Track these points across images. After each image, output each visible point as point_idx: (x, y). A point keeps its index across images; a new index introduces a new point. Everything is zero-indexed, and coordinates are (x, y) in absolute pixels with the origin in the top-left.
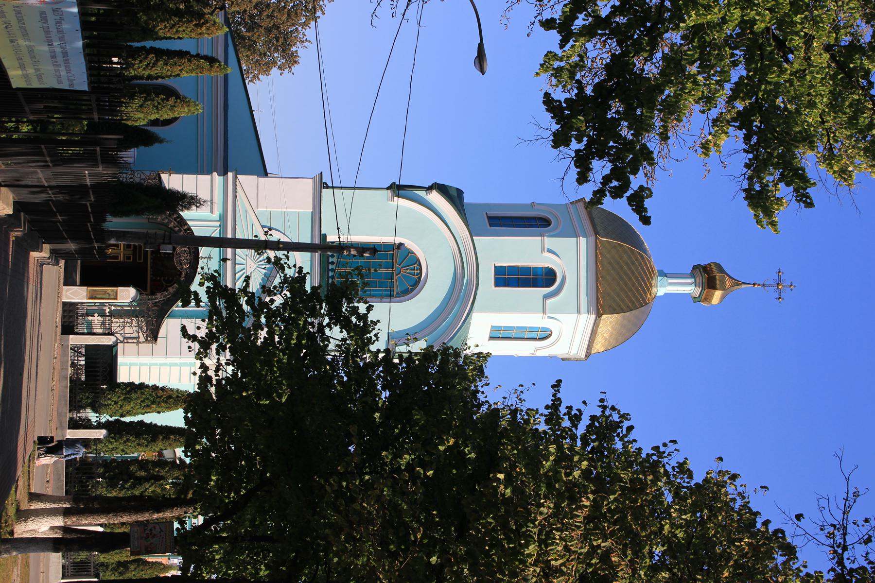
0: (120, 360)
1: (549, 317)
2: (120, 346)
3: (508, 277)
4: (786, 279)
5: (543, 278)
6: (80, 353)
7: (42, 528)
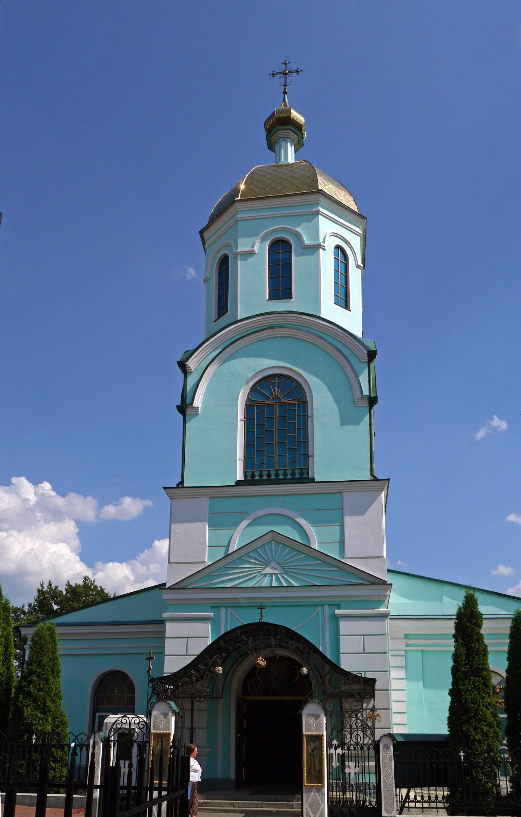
1: (324, 242)
3: (281, 285)
4: (279, 67)
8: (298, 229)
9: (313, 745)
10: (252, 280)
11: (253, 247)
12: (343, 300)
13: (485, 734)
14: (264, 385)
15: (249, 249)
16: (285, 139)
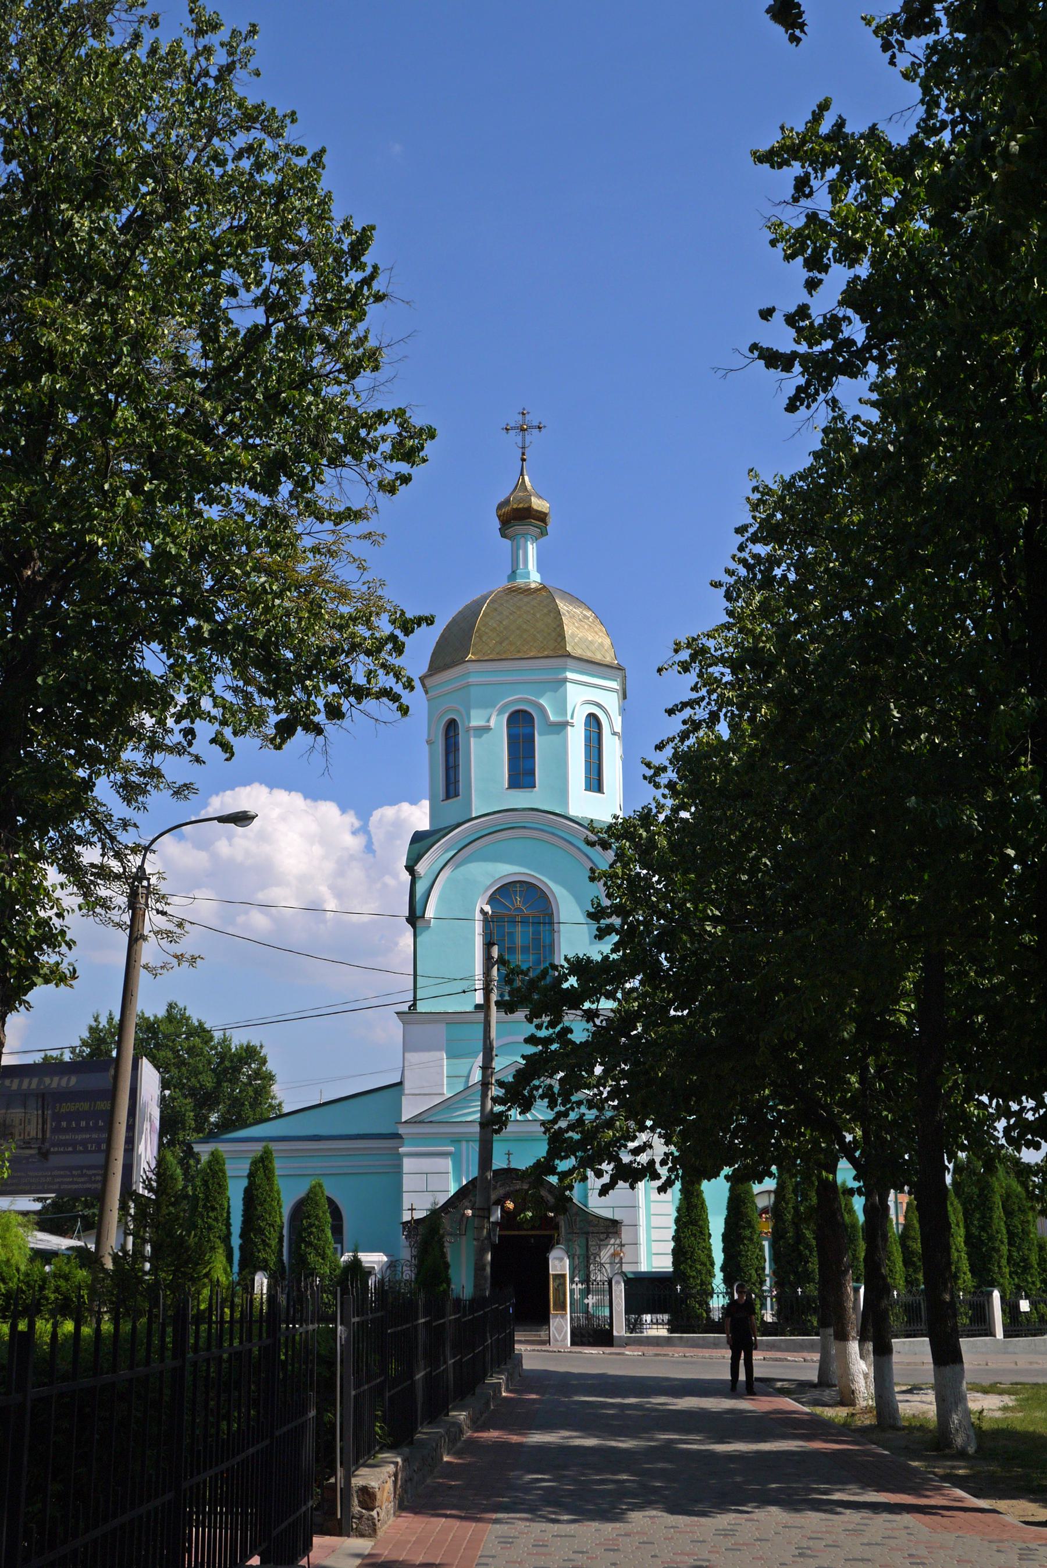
0: (644, 1268)
1: (572, 717)
2: (626, 1268)
3: (522, 775)
4: (515, 420)
5: (522, 728)
6: (636, 1320)
7: (861, 1368)
8: (542, 701)
9: (558, 1282)
10: (487, 756)
11: (488, 721)
12: (595, 783)
13: (699, 1272)
14: (503, 893)
15: (482, 723)
16: (524, 535)
